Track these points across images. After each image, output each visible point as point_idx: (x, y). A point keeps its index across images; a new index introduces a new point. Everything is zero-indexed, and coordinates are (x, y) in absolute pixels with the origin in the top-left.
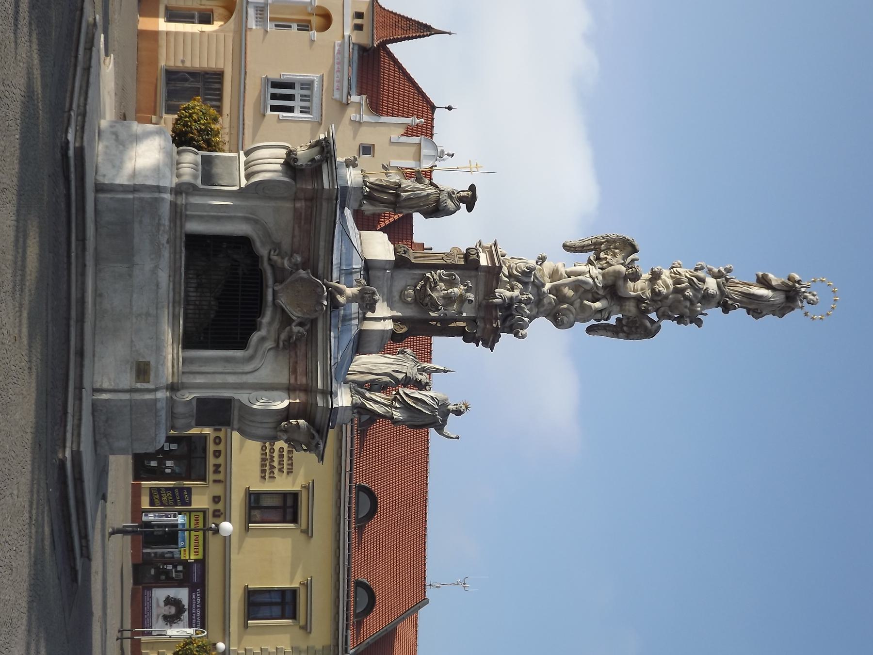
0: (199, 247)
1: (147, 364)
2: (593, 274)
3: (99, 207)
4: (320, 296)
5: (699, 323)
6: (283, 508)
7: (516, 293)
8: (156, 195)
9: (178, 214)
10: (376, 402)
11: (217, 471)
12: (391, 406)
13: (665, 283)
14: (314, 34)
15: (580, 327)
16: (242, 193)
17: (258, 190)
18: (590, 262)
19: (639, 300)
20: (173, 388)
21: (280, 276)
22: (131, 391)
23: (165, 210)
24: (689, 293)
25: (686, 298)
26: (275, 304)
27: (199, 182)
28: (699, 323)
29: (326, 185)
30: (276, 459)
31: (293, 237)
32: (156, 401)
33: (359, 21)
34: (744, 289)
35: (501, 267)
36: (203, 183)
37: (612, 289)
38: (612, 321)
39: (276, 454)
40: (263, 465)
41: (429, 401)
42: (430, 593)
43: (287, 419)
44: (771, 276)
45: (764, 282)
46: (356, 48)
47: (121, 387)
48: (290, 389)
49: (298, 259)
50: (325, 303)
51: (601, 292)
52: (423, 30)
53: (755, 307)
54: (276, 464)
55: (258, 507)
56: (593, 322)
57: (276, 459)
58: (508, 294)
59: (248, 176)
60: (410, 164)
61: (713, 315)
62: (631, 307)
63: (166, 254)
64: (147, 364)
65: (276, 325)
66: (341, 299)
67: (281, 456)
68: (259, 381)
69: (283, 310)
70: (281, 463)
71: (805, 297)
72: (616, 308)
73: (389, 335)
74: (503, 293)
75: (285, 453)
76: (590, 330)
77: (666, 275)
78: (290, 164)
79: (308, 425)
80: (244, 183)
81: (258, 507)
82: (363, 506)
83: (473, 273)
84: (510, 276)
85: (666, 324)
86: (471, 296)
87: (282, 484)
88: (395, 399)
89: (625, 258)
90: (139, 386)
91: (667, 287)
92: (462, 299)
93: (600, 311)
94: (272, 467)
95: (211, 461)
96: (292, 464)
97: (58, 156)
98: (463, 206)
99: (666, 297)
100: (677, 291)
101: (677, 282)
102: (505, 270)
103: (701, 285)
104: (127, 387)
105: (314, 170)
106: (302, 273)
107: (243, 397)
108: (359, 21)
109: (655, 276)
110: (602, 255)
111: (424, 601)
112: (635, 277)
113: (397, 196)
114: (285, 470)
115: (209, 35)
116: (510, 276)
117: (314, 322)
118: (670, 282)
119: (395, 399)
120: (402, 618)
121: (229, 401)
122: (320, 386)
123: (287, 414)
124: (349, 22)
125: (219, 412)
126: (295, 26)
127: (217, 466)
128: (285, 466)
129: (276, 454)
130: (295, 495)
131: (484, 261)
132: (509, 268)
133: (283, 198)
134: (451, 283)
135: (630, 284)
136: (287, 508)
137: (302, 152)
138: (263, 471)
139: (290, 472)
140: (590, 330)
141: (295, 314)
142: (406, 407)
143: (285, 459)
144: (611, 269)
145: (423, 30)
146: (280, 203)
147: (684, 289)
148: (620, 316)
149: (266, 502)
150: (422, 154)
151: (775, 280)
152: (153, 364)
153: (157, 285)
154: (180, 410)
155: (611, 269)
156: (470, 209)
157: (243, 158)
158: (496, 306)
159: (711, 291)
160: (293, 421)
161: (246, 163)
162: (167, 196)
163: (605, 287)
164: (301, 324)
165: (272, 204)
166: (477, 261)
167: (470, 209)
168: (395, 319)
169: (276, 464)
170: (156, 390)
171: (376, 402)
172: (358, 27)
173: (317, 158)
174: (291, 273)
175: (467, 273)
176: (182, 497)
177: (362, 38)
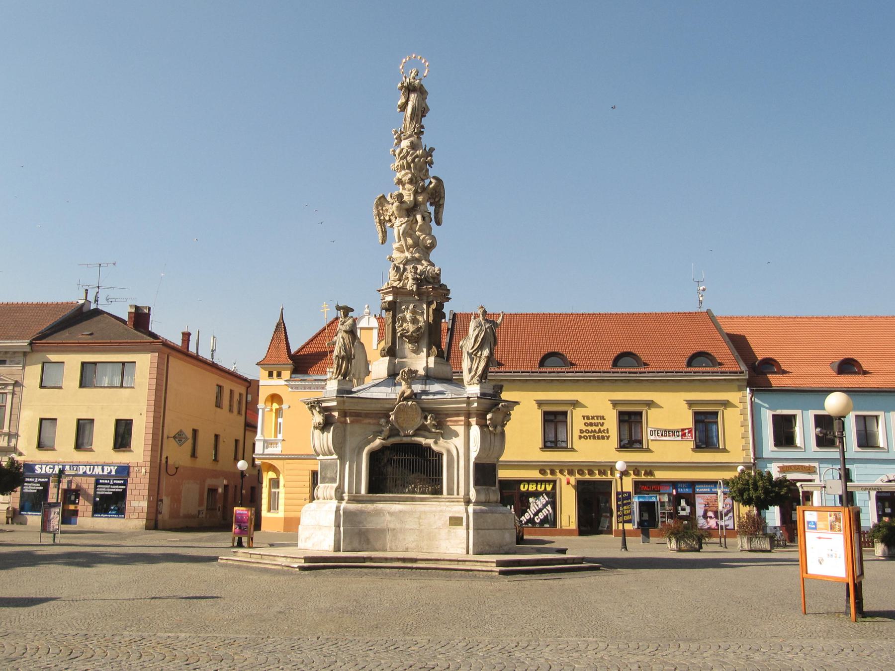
0: (379, 484)
1: (451, 518)
2: (399, 225)
3: (349, 549)
4: (406, 406)
5: (432, 150)
6: (629, 422)
7: (410, 276)
8: (341, 512)
9: (354, 499)
10: (477, 368)
11: (605, 473)
12: (480, 357)
13: (404, 176)
14: (285, 406)
15: (435, 229)
16: (342, 458)
17: (339, 446)
18: (392, 226)
19: (416, 193)
20: (468, 502)
21: (394, 432)
22: (468, 528)
23: (353, 506)
24: (409, 158)
25: (413, 161)
26: (414, 435)
27: (335, 485)
28: (432, 150)
29: (335, 403)
30: (594, 428)
31: (369, 423)
32: (475, 512)
33: (275, 373)
34: (408, 120)
35: (393, 287)
36: (335, 482)
37: (410, 211)
38: (431, 209)
39: (590, 428)
40: (599, 438)
41: (476, 332)
42: (704, 310)
43: (487, 426)
44: (399, 103)
45: (403, 107)
46: (293, 376)
47: (465, 536)
48: (468, 425)
49: (383, 421)
50: (410, 403)
51: (411, 218)
52: (281, 327)
53: (420, 113)
54: (597, 428)
55: (631, 440)
56: (433, 224)
57: (594, 428)
58: (411, 281)
59: (331, 454)
60: (375, 333)
61: (427, 141)
62: (420, 198)
63: (380, 506)
64: (451, 518)
65: (427, 434)
66: (408, 392)
67: (591, 424)
68: (461, 446)
69: (418, 429)
70: (591, 424)
71: (414, 78)
72: (422, 207)
73: (439, 359)
74: (410, 285)
75: (588, 421)
76: (438, 223)
77: (399, 175)
78: (324, 427)
79: (492, 412)
80: (335, 456)
81: (631, 440)
82: (553, 364)
83: (398, 305)
84: (400, 280)
85: (432, 172)
86: (411, 306)
87: (612, 423)
88: (476, 355)
89: (388, 203)
90: (464, 524)
91: (406, 174)
92: (414, 312)
93: (424, 218)
94: (600, 431)
95: (597, 477)
96: (597, 417)
97: (307, 572)
98: (350, 314)
99: (413, 175)
100: (409, 167)
101: (403, 168)
102: (395, 284)
103: (405, 151)
104: (465, 531)
105: (325, 411)
106: (392, 417)
107: (474, 455)
108: (275, 373)
109: (400, 182)
110: (387, 218)
111: (708, 312)
112: (400, 197)
113: (343, 358)
114: (601, 421)
115: (286, 481)
116: (400, 280)
117: (424, 410)
118: (403, 172)
119: (476, 355)
120: (719, 329)
121: (477, 465)
122: (465, 405)
123: (483, 426)
124: (275, 381)
125: (485, 473)
126: (280, 420)
127: (646, 474)
128: (599, 421)
129: (590, 428)
130: (621, 414)
131: (390, 298)
132: (395, 281)
133: (345, 430)
134: (404, 320)
135: (406, 198)
136: (630, 421)
137: (318, 418)
138: (603, 438)
139: (603, 418)
140: (438, 223)
141: (418, 422)
142: (481, 348)
143: (593, 421)
144: (395, 213)
145: (281, 327)
146: (348, 433)
147: (407, 162)
148: (428, 204)
149: (551, 437)
150: (367, 326)
151: (402, 100)
152: (451, 515)
153: (401, 512)
154: (483, 498)
155: (395, 213)
156: (352, 310)
157: (321, 457)
158: (418, 288)
159: (409, 144)
160: (488, 422)
161: (324, 455)
162: (343, 505)
163: (408, 216)
164: (426, 418)
165: (348, 437)
166: (390, 303)
167: (352, 310)
168: (428, 355)
169: (597, 428)
170: (467, 512)
171: (477, 368)
172: (279, 375)
173: (318, 409)
174: (392, 425)
175: (398, 309)
176: (624, 498)
177: (286, 374)
